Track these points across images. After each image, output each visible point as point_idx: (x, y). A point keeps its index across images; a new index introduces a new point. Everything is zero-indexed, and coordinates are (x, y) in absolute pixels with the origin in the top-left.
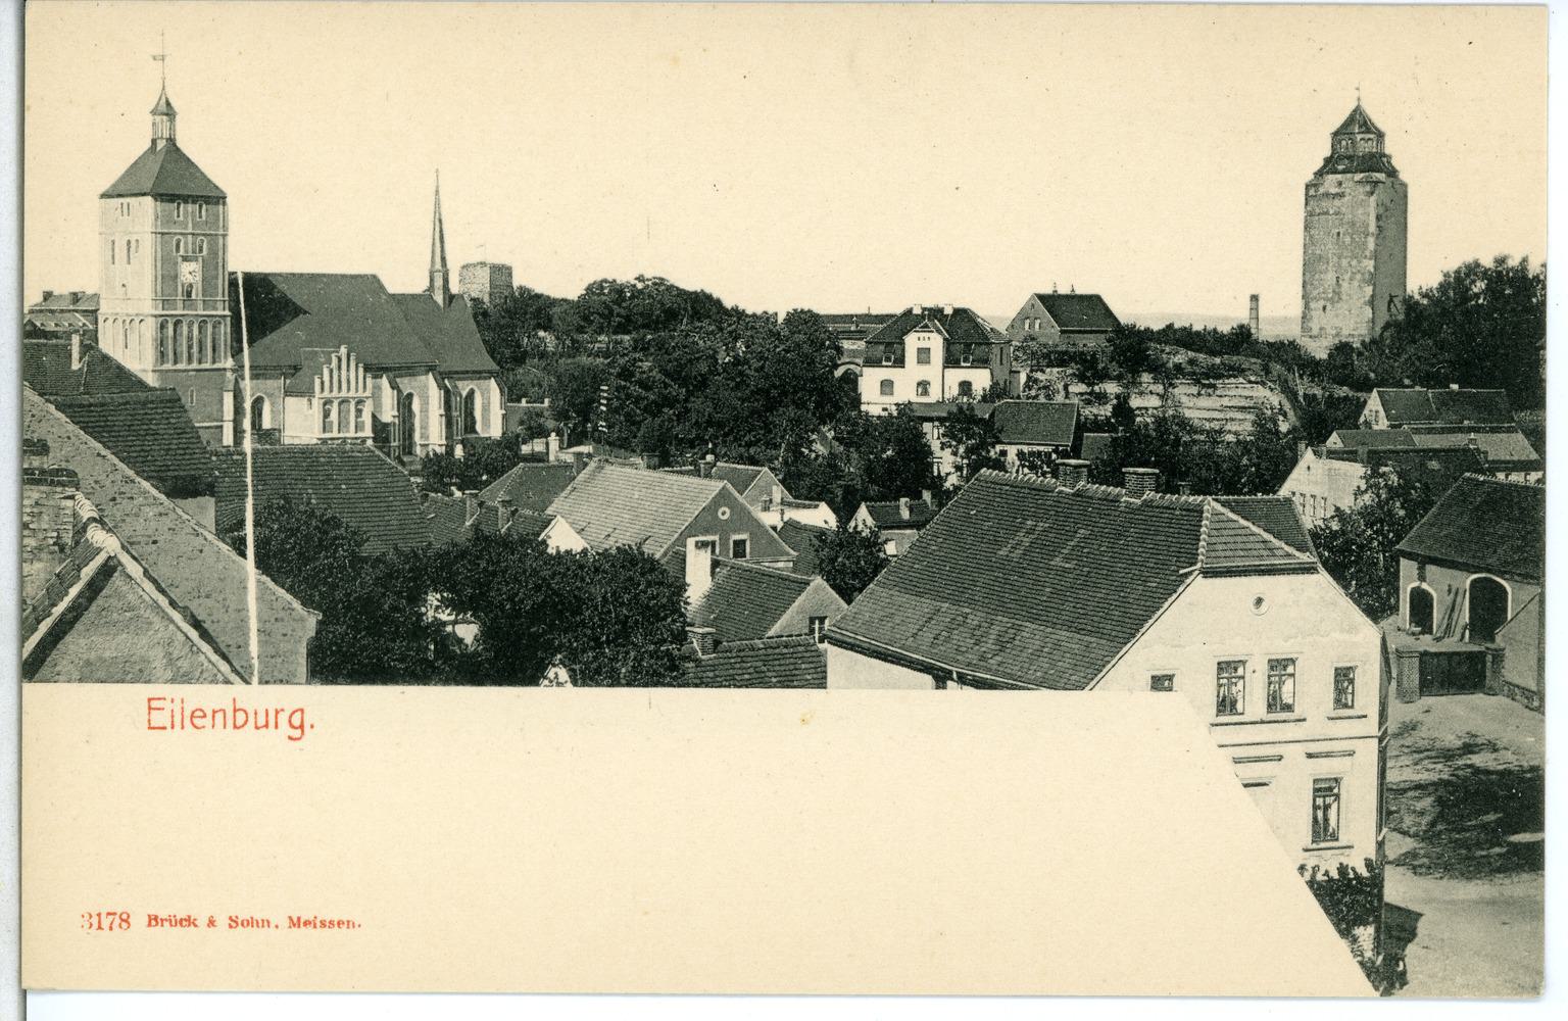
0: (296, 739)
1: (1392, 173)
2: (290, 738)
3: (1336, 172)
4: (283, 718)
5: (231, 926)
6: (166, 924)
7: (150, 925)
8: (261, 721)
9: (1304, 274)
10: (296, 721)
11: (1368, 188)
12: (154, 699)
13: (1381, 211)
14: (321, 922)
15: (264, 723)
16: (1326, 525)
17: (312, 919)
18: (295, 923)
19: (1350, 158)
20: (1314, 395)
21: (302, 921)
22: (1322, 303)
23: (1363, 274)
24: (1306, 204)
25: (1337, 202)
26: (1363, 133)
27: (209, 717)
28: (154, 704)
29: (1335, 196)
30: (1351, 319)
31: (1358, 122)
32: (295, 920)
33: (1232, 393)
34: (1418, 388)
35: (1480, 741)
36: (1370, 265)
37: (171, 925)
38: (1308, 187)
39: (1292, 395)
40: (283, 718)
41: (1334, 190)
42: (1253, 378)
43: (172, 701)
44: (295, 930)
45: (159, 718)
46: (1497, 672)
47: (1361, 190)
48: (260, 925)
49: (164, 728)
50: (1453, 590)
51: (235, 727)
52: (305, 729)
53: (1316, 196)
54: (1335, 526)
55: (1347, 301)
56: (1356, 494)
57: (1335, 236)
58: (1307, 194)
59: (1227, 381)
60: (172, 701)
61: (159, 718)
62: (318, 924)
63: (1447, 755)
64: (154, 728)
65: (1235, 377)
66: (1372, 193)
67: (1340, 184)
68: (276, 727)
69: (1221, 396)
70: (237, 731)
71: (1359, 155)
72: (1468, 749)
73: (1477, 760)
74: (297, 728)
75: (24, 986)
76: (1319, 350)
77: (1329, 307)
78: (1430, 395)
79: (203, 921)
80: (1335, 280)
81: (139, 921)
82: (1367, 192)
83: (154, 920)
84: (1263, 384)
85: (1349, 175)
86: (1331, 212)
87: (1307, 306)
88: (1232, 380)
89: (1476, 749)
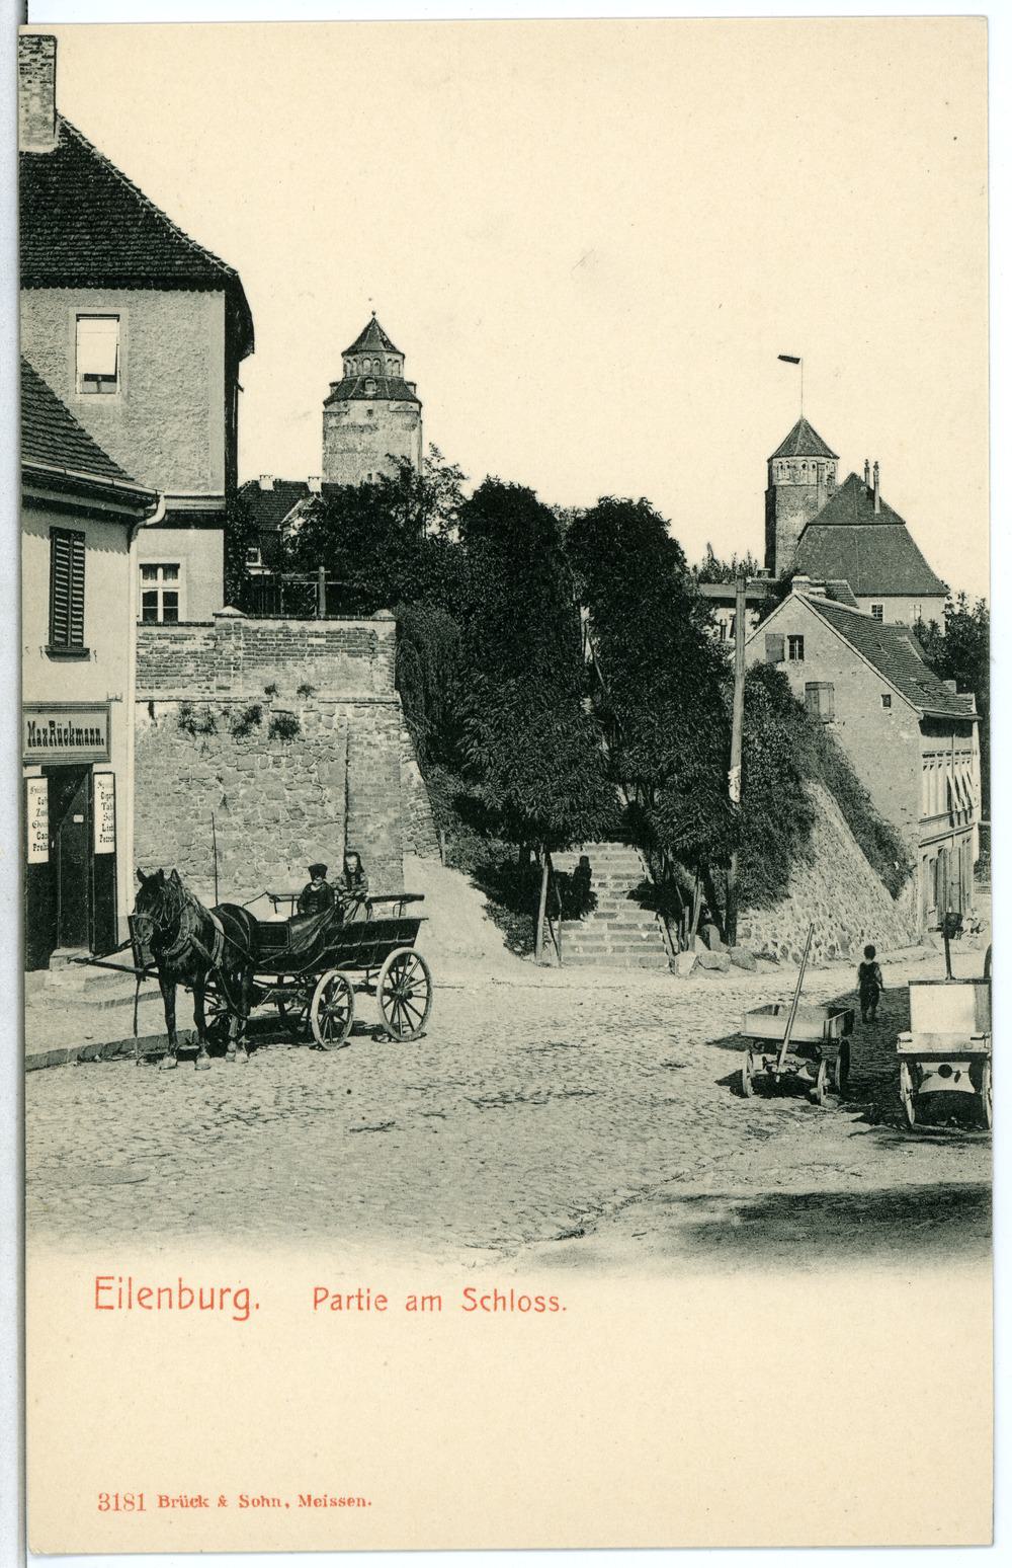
0: (241, 1319)
2: (235, 1318)
4: (228, 1298)
6: (178, 1505)
7: (161, 1505)
8: (207, 1302)
10: (241, 1301)
12: (102, 1278)
15: (351, 1301)
17: (321, 1496)
18: (307, 1501)
21: (313, 1499)
24: (325, 438)
25: (366, 437)
27: (155, 1293)
28: (102, 1283)
29: (362, 429)
31: (371, 341)
32: (306, 1499)
37: (182, 1505)
40: (228, 1298)
41: (363, 421)
43: (121, 1280)
44: (305, 1508)
45: (107, 1298)
49: (111, 1308)
51: (181, 1307)
58: (325, 426)
60: (121, 1280)
61: (107, 1298)
62: (328, 1503)
64: (101, 1307)
67: (370, 412)
68: (221, 1307)
70: (183, 1311)
79: (283, 1504)
81: (151, 1502)
83: (164, 1501)
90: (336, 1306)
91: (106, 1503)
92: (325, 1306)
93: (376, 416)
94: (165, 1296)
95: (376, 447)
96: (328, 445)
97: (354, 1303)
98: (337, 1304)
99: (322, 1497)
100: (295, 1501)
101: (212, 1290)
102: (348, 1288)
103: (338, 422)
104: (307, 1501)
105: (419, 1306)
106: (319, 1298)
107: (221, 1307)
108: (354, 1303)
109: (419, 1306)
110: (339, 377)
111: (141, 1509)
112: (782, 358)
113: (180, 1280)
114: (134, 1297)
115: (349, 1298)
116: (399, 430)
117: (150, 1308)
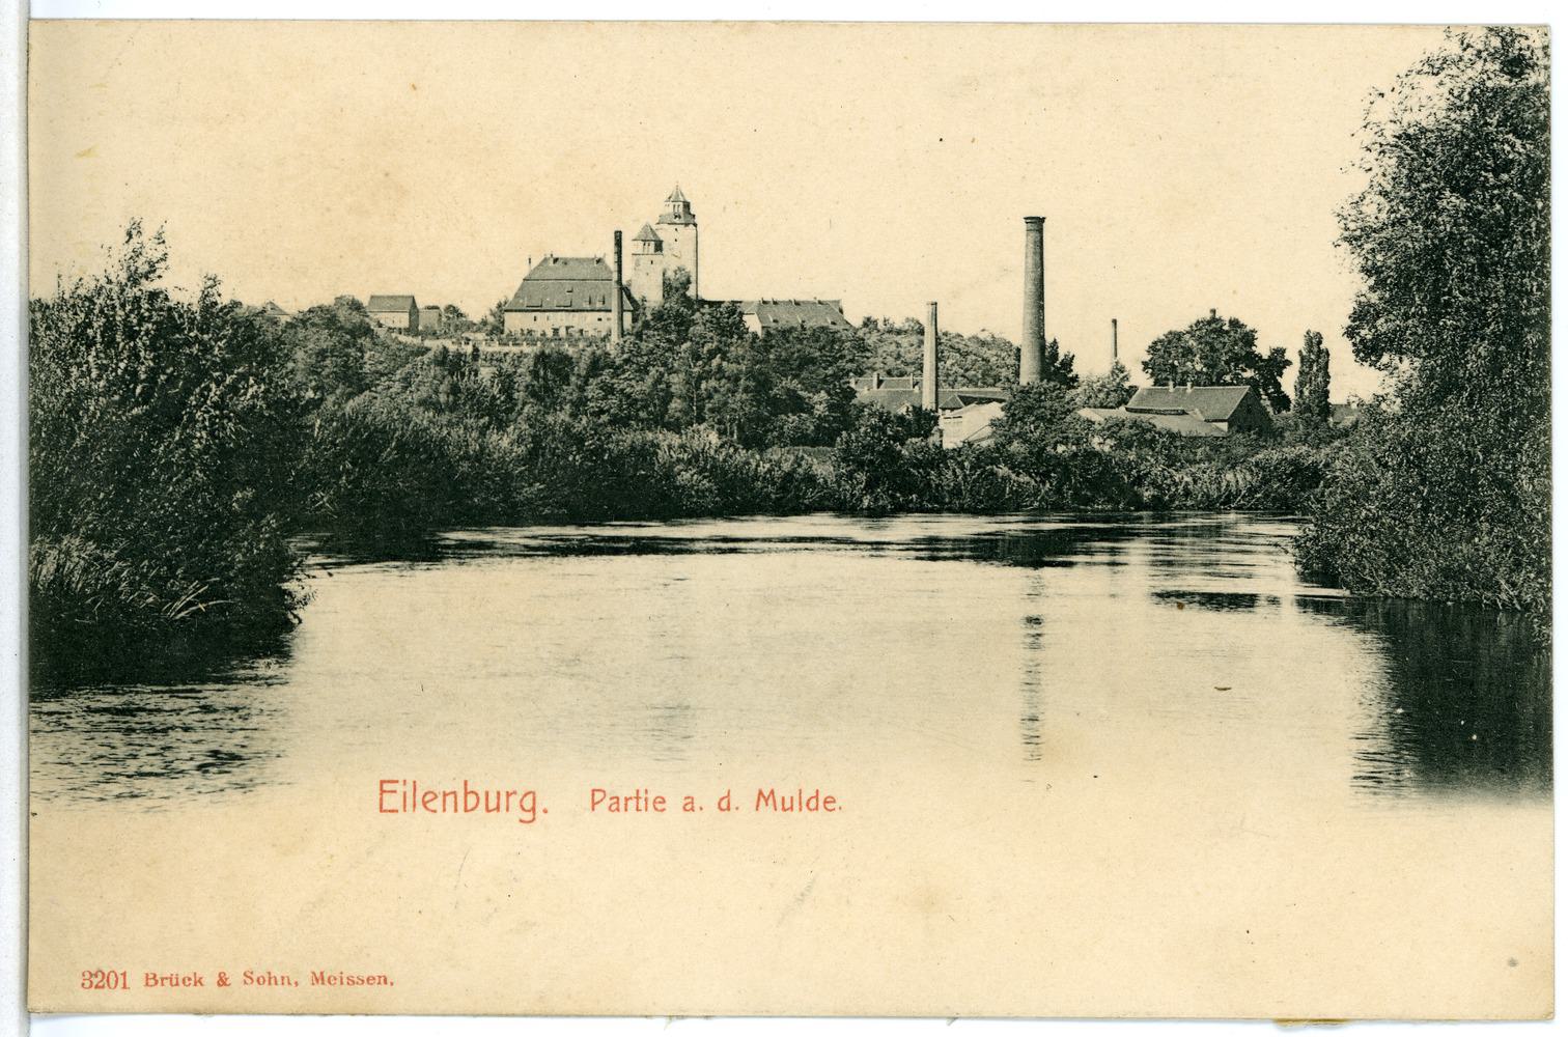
2: (521, 821)
5: (245, 982)
6: (167, 982)
8: (492, 805)
10: (528, 804)
14: (348, 978)
15: (448, 798)
17: (337, 975)
27: (440, 798)
32: (318, 975)
40: (514, 801)
48: (279, 982)
49: (397, 811)
51: (466, 810)
52: (463, 791)
61: (391, 801)
62: (345, 981)
64: (385, 811)
70: (469, 814)
74: (472, 792)
75: (571, 264)
79: (389, 981)
90: (724, 804)
92: (603, 807)
94: (450, 799)
97: (632, 804)
98: (616, 804)
99: (337, 975)
100: (305, 981)
101: (498, 793)
102: (445, 780)
104: (319, 979)
105: (622, 806)
106: (596, 800)
107: (507, 810)
108: (632, 804)
109: (622, 806)
111: (125, 987)
113: (466, 783)
114: (419, 799)
115: (627, 799)
117: (435, 811)
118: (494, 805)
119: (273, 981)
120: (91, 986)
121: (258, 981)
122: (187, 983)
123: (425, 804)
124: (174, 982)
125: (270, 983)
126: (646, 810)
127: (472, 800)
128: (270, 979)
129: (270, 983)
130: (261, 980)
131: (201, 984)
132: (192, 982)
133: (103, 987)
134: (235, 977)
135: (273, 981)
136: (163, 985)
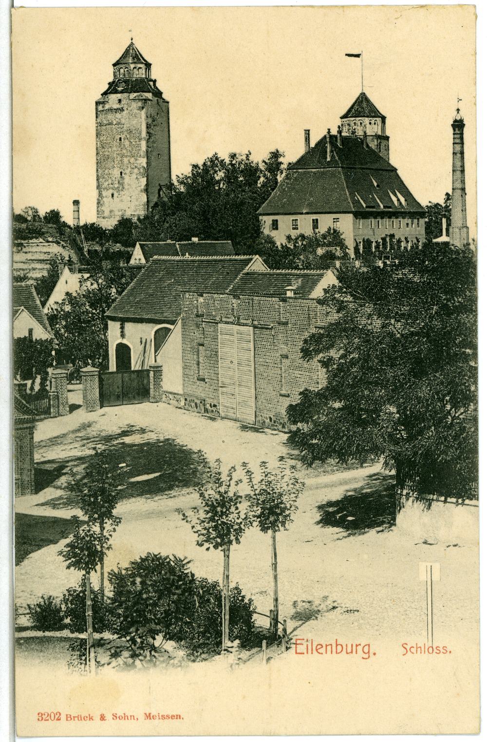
1: (158, 94)
2: (363, 658)
3: (116, 92)
5: (113, 719)
6: (76, 719)
7: (67, 720)
8: (349, 650)
9: (97, 170)
10: (366, 650)
11: (140, 104)
13: (150, 121)
16: (61, 308)
19: (126, 82)
20: (96, 250)
22: (111, 191)
23: (139, 169)
24: (97, 117)
25: (118, 115)
26: (135, 63)
27: (324, 646)
29: (117, 110)
30: (132, 202)
31: (132, 55)
32: (148, 715)
33: (34, 249)
34: (169, 241)
35: (134, 429)
36: (143, 162)
38: (97, 103)
39: (79, 250)
40: (360, 648)
42: (50, 239)
46: (158, 385)
47: (135, 106)
49: (304, 653)
50: (144, 341)
53: (103, 111)
54: (68, 308)
55: (128, 189)
56: (80, 282)
57: (118, 141)
58: (97, 109)
59: (30, 241)
63: (108, 439)
65: (36, 238)
66: (143, 108)
69: (26, 253)
71: (133, 80)
72: (125, 433)
73: (128, 440)
76: (108, 224)
77: (116, 195)
78: (178, 246)
79: (135, 718)
80: (120, 174)
82: (140, 107)
84: (58, 243)
85: (126, 95)
86: (114, 123)
87: (100, 195)
88: (34, 240)
89: (130, 434)
91: (41, 717)
93: (122, 102)
95: (123, 121)
96: (98, 121)
100: (142, 717)
103: (103, 107)
104: (149, 716)
110: (111, 79)
112: (346, 55)
116: (136, 111)
117: (322, 654)
118: (352, 651)
119: (126, 718)
120: (42, 719)
121: (119, 717)
122: (86, 719)
123: (317, 650)
124: (80, 719)
125: (125, 719)
126: (307, 653)
127: (339, 648)
128: (125, 717)
129: (125, 719)
130: (121, 718)
131: (146, 714)
132: (88, 719)
133: (48, 720)
134: (109, 716)
135: (126, 718)
136: (74, 720)
